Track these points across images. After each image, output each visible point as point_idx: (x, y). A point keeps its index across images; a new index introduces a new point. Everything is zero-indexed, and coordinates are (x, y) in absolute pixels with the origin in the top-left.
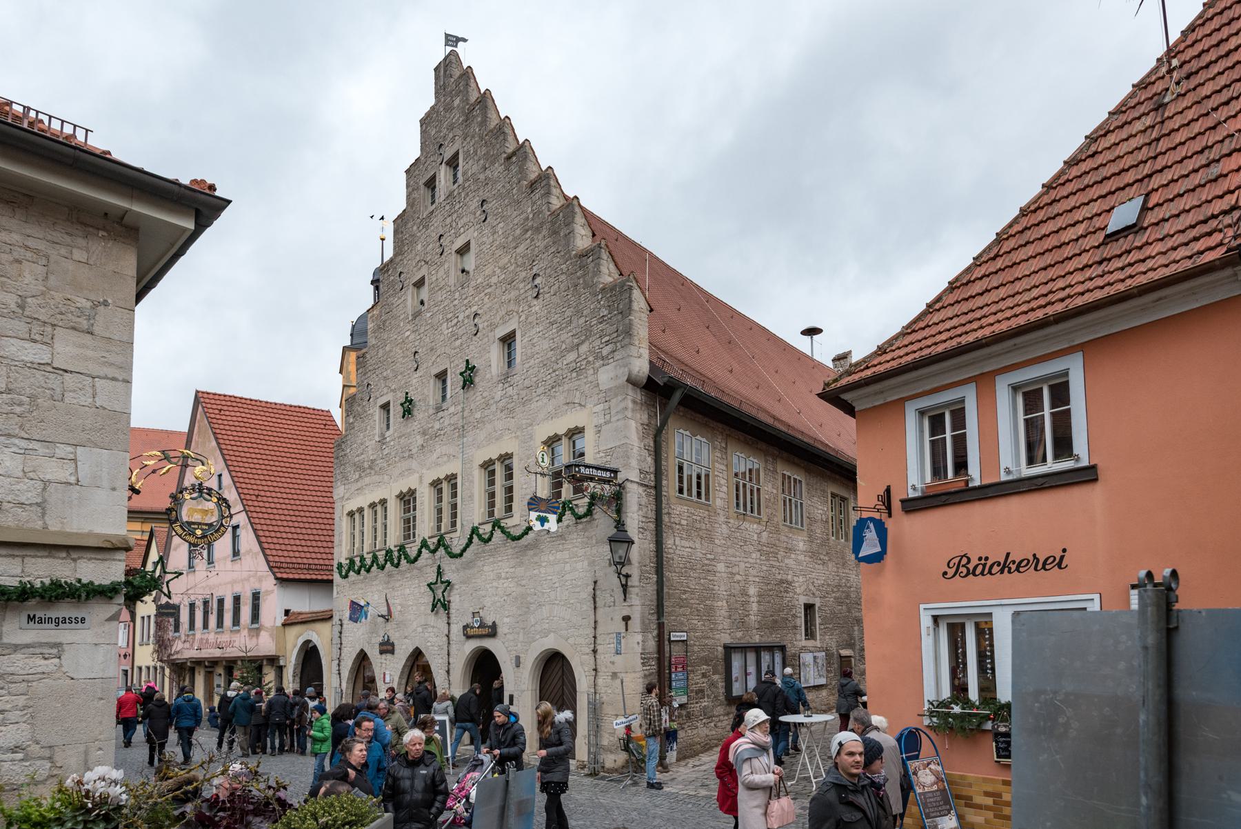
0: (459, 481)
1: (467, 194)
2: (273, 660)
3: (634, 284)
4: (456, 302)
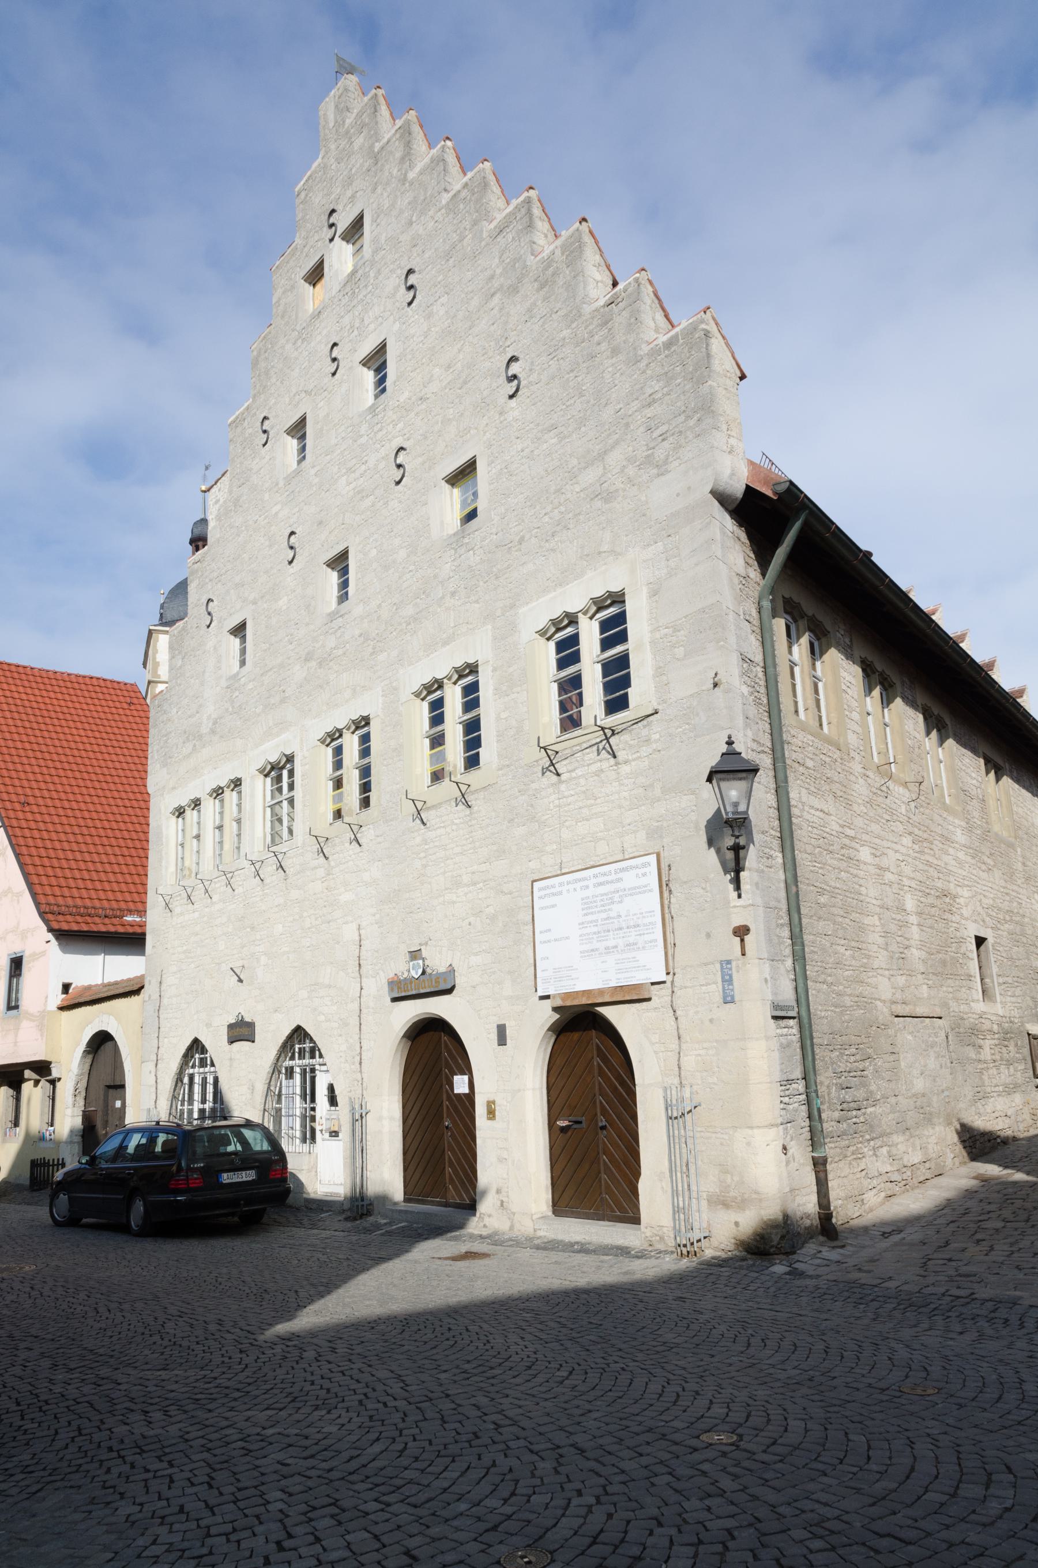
0: (374, 729)
1: (379, 272)
2: (42, 1068)
3: (714, 329)
4: (363, 440)
